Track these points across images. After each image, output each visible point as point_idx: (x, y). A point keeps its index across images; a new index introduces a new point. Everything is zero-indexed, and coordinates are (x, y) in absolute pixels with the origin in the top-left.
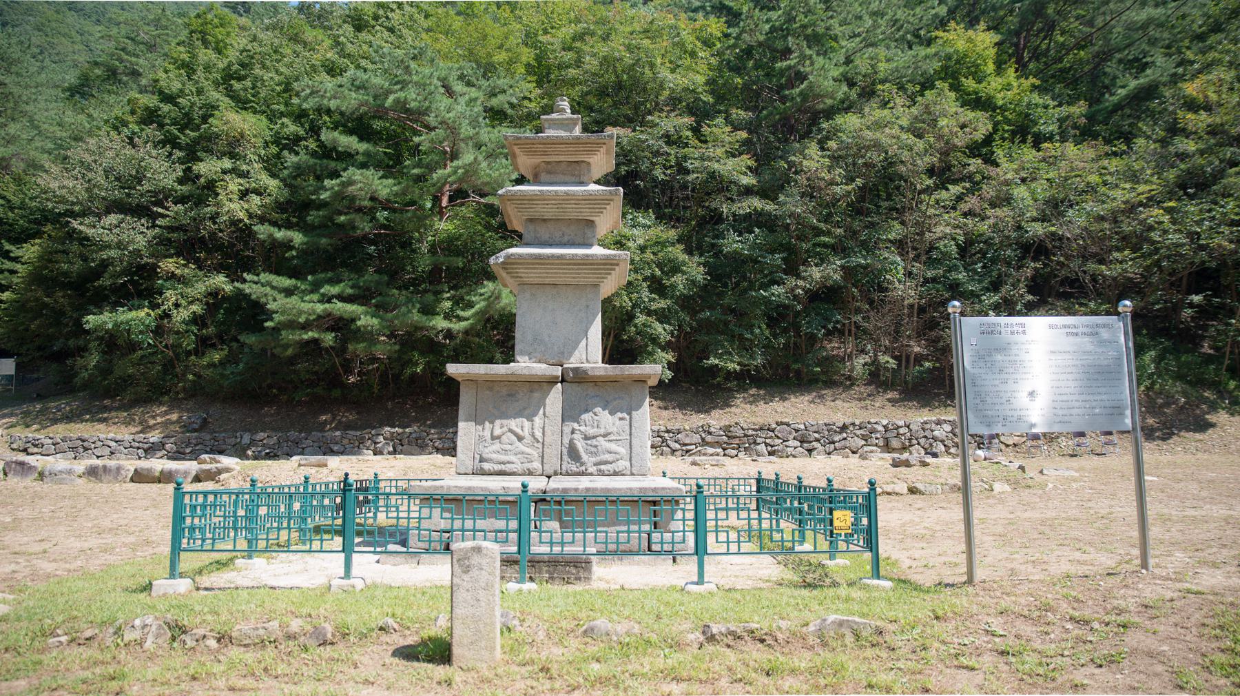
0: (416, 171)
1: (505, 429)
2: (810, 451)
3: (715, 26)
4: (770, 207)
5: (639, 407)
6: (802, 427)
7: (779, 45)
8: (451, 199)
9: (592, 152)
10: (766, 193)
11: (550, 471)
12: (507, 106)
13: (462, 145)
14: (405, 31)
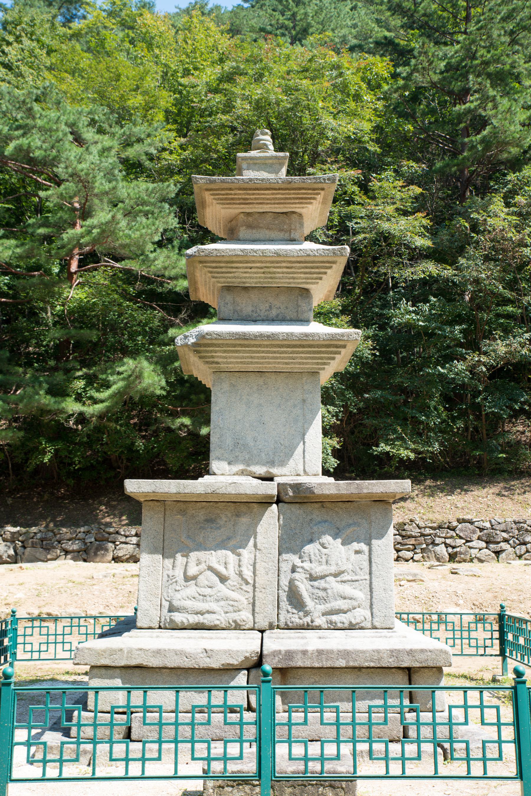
0: (42, 231)
1: (203, 566)
2: (498, 553)
3: (381, 66)
4: (448, 272)
5: (381, 536)
6: (488, 525)
7: (457, 86)
8: (82, 263)
9: (307, 200)
10: (437, 255)
11: (263, 623)
12: (144, 157)
13: (96, 201)
14: (24, 69)
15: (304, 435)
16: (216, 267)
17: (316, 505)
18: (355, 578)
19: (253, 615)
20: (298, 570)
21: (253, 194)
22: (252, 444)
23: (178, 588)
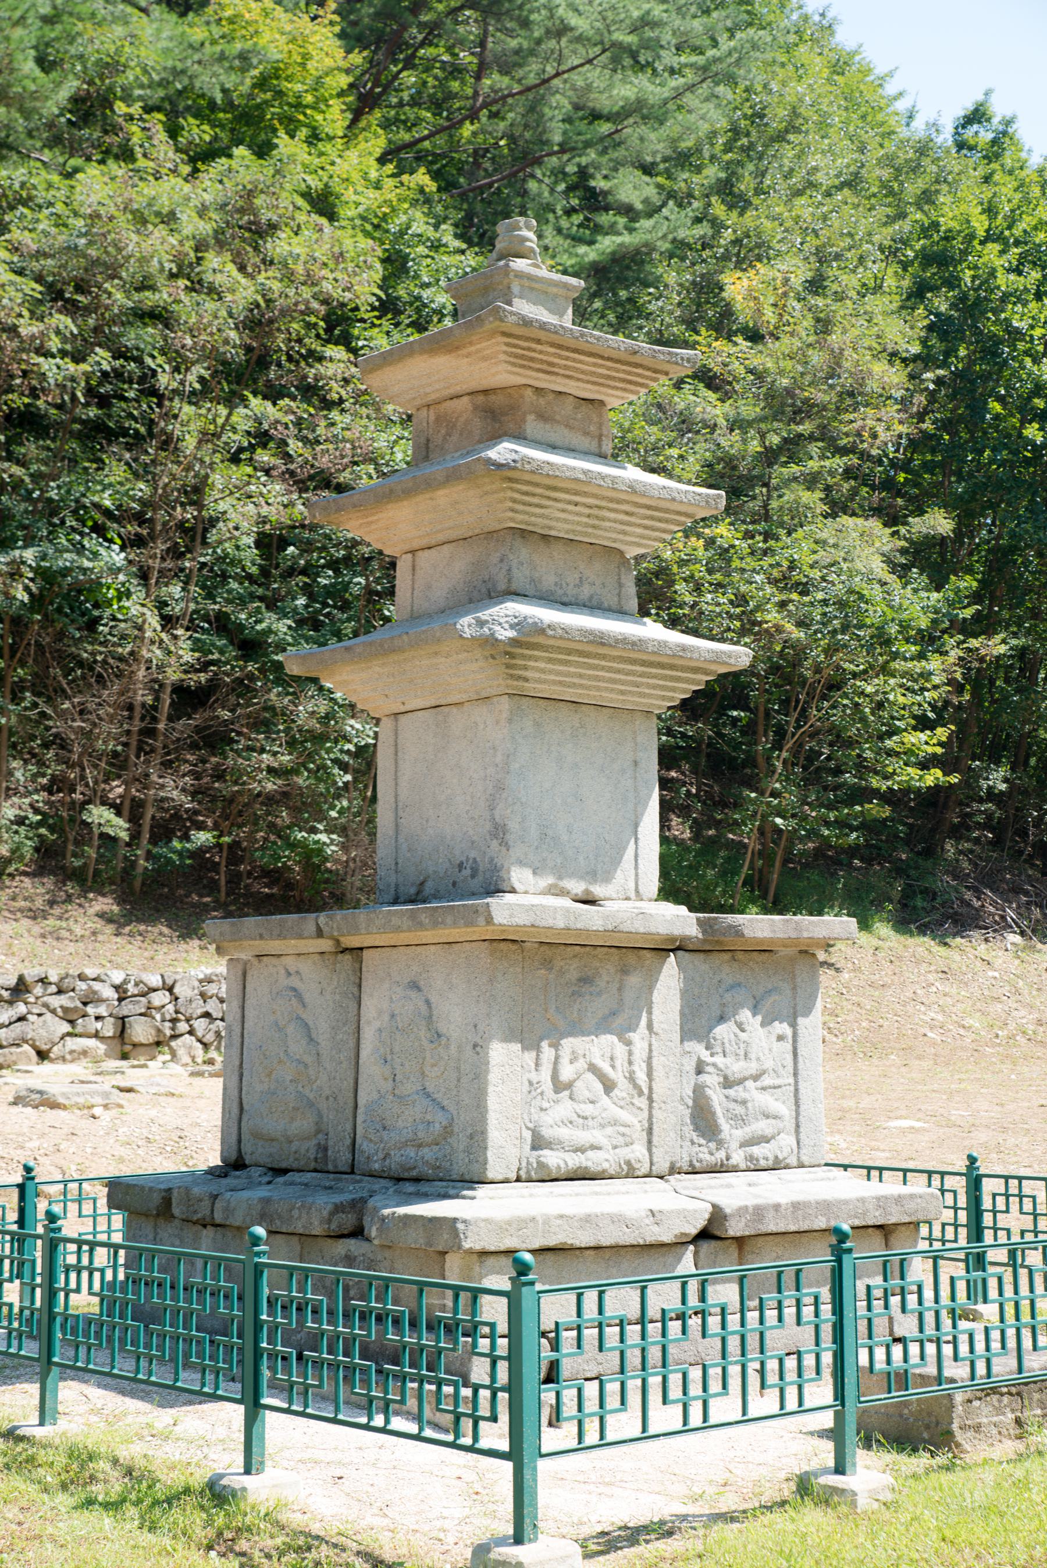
1: (581, 1064)
5: (808, 1012)
15: (636, 825)
16: (527, 494)
17: (726, 956)
18: (777, 1082)
19: (650, 1150)
20: (709, 1069)
21: (567, 358)
22: (565, 837)
23: (545, 1105)
